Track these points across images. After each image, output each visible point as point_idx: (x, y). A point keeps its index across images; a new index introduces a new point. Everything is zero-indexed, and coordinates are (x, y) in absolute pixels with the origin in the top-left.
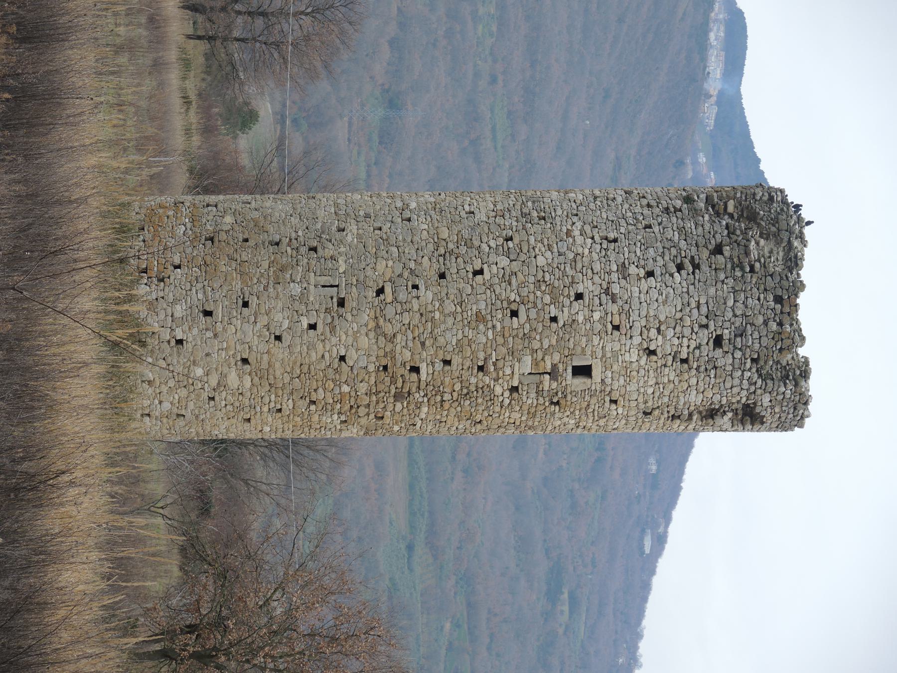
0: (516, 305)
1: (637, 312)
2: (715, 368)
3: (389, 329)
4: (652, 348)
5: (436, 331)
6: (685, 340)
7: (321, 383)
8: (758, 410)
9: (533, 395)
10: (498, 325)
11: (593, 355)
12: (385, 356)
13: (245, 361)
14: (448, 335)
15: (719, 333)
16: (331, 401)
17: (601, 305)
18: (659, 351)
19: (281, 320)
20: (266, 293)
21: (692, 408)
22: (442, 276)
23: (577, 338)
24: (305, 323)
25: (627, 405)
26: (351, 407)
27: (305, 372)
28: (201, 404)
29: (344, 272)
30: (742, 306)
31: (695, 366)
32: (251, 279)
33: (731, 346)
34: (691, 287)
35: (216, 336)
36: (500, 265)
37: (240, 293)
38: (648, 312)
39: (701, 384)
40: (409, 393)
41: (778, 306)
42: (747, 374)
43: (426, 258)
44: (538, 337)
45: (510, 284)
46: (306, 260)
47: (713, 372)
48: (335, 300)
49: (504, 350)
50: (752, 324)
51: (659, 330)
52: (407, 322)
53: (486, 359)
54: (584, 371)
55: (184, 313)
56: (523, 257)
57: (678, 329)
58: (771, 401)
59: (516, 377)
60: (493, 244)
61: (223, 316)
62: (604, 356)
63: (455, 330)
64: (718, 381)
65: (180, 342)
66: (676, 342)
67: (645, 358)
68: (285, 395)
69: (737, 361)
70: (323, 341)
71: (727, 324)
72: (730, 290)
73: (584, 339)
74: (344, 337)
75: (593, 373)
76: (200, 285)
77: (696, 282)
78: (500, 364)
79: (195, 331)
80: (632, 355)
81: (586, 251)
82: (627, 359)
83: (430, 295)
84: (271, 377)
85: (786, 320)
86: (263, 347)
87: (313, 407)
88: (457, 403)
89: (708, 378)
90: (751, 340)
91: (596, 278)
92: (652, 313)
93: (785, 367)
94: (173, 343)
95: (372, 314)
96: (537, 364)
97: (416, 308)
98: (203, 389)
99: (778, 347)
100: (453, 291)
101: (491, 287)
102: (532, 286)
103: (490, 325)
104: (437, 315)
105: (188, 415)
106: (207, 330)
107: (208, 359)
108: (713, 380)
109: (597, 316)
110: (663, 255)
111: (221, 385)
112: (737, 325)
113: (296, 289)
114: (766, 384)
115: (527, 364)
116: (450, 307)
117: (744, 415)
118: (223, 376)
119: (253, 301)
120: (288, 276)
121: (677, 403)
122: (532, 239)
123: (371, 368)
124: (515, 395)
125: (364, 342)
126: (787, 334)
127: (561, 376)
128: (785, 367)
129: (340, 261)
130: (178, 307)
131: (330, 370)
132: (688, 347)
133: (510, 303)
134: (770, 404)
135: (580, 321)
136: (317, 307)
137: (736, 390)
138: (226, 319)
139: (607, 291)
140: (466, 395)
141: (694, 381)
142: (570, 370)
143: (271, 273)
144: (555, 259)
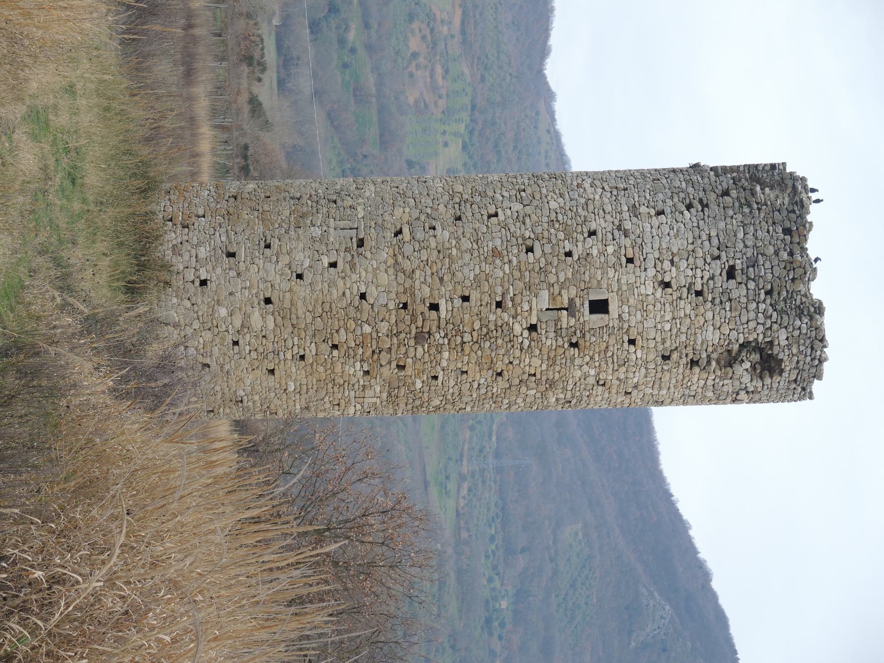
0: (531, 241)
1: (649, 245)
2: (730, 300)
3: (407, 265)
4: (667, 280)
5: (453, 266)
6: (699, 271)
7: (342, 322)
8: (776, 350)
9: (552, 335)
10: (514, 260)
11: (609, 289)
12: (405, 292)
13: (268, 301)
14: (466, 270)
15: (731, 263)
16: (353, 345)
17: (614, 240)
18: (673, 284)
19: (303, 260)
20: (287, 236)
21: (710, 349)
22: (459, 218)
23: (592, 270)
24: (326, 261)
25: (645, 345)
26: (373, 352)
27: (327, 311)
28: (225, 349)
29: (363, 218)
30: (752, 237)
31: (710, 299)
32: (273, 224)
33: (744, 277)
34: (701, 222)
35: (239, 274)
36: (514, 209)
37: (262, 236)
38: (661, 245)
39: (717, 318)
40: (429, 333)
41: (788, 238)
42: (762, 307)
43: (442, 206)
44: (554, 271)
45: (524, 224)
46: (325, 210)
47: (728, 304)
48: (354, 240)
49: (521, 285)
50: (763, 254)
51: (672, 262)
52: (425, 259)
53: (503, 294)
54: (600, 307)
55: (208, 254)
56: (535, 203)
57: (691, 260)
58: (787, 339)
59: (534, 313)
60: (506, 194)
61: (246, 256)
62: (619, 289)
63: (472, 265)
64: (733, 315)
65: (204, 283)
66: (690, 273)
67: (660, 290)
68: (308, 338)
69: (751, 292)
70: (344, 278)
71: (739, 255)
72: (740, 224)
73: (599, 272)
74: (363, 274)
75: (611, 308)
76: (223, 230)
77: (706, 218)
78: (518, 299)
79: (219, 271)
80: (648, 287)
81: (597, 197)
82: (643, 292)
83: (447, 234)
84: (294, 316)
85: (797, 251)
86: (285, 286)
87: (335, 353)
88: (477, 346)
89: (723, 311)
90: (763, 269)
91: (608, 217)
92: (664, 246)
93: (799, 307)
94: (197, 283)
95: (391, 252)
96: (554, 299)
97: (433, 245)
98: (227, 331)
99: (791, 277)
100: (469, 231)
101: (506, 227)
102: (546, 225)
103: (506, 260)
104: (454, 252)
105: (213, 365)
106: (230, 269)
107: (232, 298)
108: (728, 313)
109: (610, 249)
110: (672, 198)
111: (245, 326)
112: (749, 255)
113: (317, 232)
114: (782, 318)
115: (544, 301)
116: (466, 244)
117: (763, 370)
118: (247, 316)
119: (275, 243)
120: (309, 222)
121: (695, 341)
122: (544, 191)
123: (392, 306)
124: (534, 334)
125: (384, 278)
126: (801, 269)
127: (579, 311)
128: (799, 307)
129: (359, 209)
130: (202, 249)
131: (352, 308)
132: (702, 278)
133: (524, 239)
134: (786, 342)
135: (595, 255)
136: (337, 246)
137: (752, 325)
138: (249, 259)
139: (619, 228)
140: (485, 336)
141: (709, 315)
142: (587, 305)
143: (292, 219)
144: (568, 203)
